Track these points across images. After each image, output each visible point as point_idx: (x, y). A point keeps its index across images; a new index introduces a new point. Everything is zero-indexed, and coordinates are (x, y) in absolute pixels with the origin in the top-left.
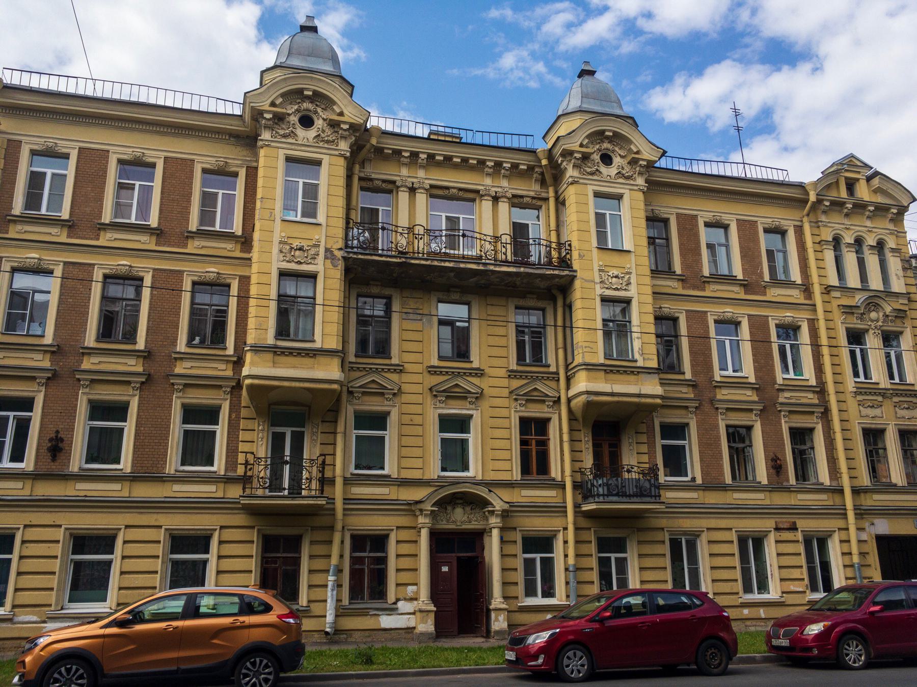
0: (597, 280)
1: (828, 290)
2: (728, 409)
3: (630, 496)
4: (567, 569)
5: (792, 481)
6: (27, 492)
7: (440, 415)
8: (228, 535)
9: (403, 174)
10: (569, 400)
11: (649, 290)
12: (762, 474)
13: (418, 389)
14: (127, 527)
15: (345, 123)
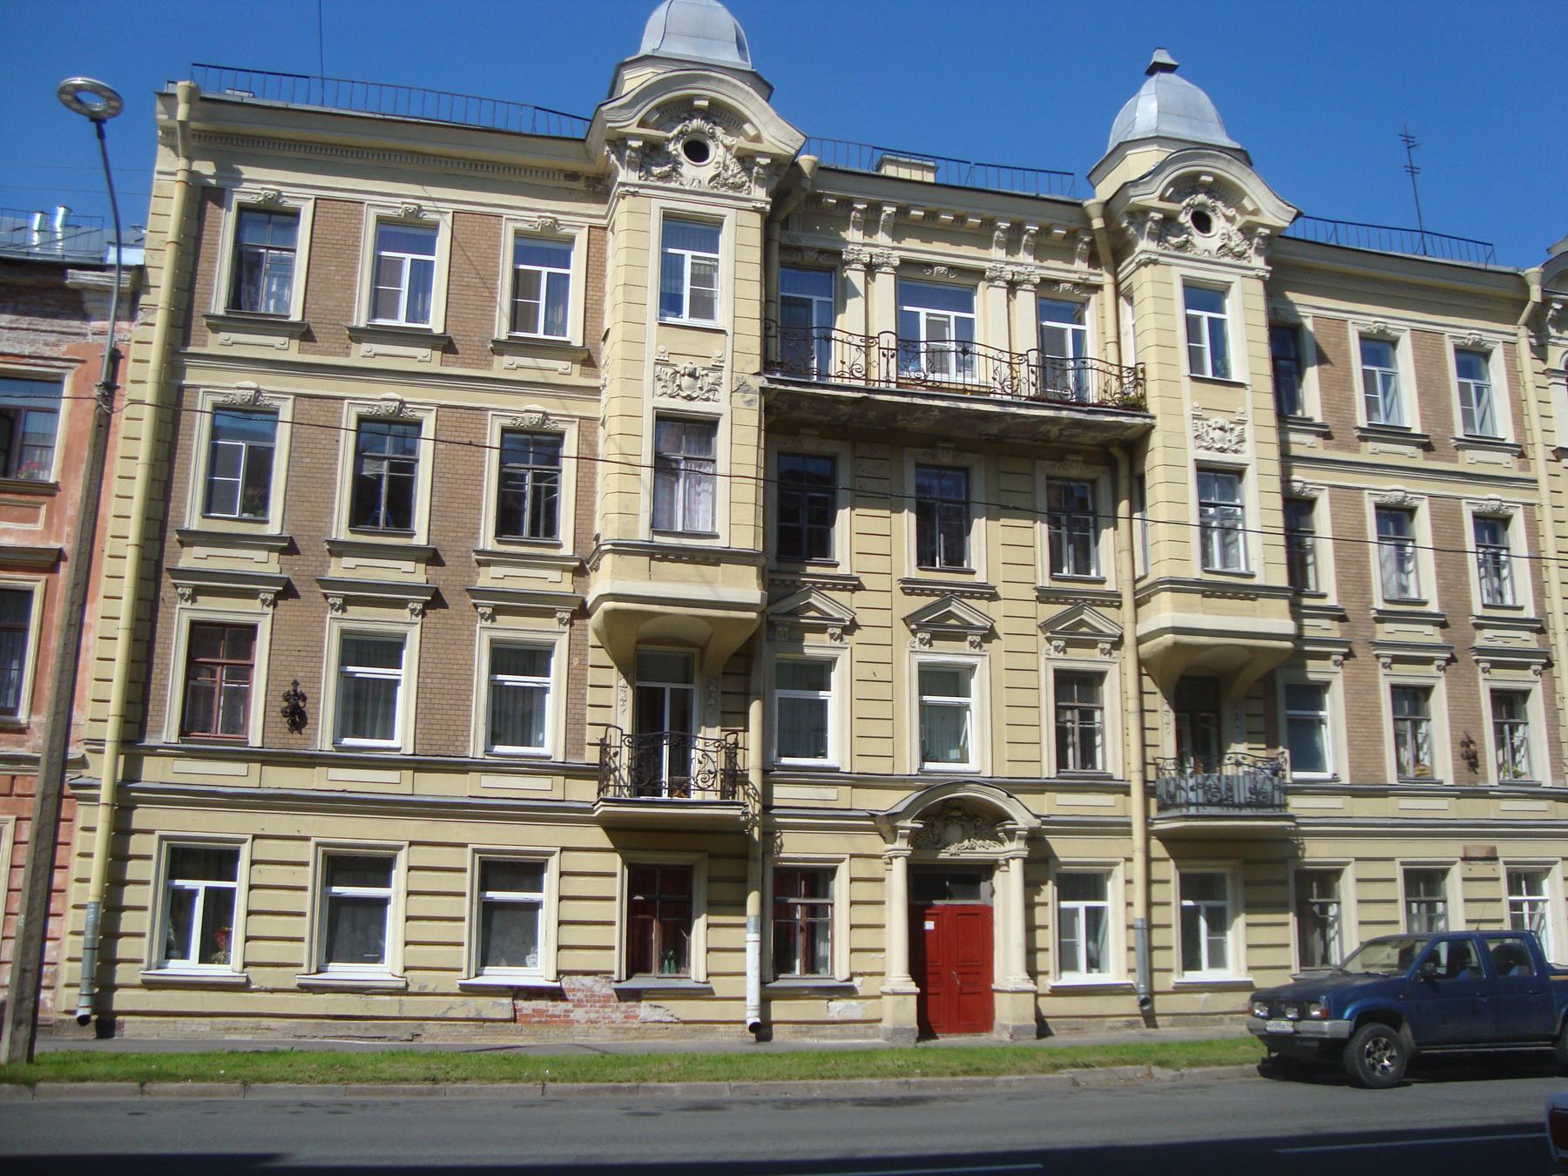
0: (1191, 434)
3: (1239, 806)
6: (253, 781)
7: (920, 665)
8: (576, 862)
13: (883, 618)
14: (412, 844)
15: (764, 154)
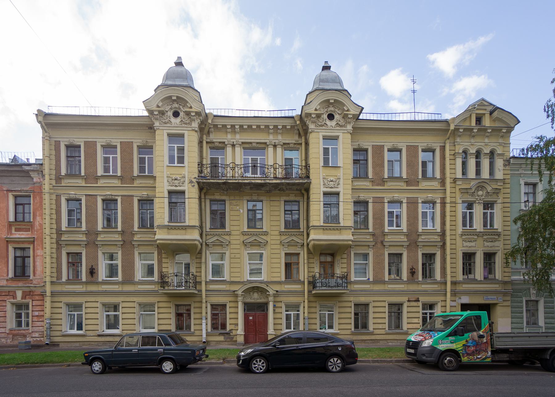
0: (322, 183)
1: (455, 180)
2: (390, 246)
4: (304, 318)
5: (420, 278)
6: (84, 289)
9: (229, 138)
10: (308, 245)
11: (350, 187)
12: (405, 275)
